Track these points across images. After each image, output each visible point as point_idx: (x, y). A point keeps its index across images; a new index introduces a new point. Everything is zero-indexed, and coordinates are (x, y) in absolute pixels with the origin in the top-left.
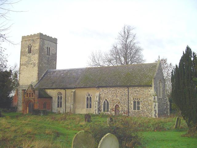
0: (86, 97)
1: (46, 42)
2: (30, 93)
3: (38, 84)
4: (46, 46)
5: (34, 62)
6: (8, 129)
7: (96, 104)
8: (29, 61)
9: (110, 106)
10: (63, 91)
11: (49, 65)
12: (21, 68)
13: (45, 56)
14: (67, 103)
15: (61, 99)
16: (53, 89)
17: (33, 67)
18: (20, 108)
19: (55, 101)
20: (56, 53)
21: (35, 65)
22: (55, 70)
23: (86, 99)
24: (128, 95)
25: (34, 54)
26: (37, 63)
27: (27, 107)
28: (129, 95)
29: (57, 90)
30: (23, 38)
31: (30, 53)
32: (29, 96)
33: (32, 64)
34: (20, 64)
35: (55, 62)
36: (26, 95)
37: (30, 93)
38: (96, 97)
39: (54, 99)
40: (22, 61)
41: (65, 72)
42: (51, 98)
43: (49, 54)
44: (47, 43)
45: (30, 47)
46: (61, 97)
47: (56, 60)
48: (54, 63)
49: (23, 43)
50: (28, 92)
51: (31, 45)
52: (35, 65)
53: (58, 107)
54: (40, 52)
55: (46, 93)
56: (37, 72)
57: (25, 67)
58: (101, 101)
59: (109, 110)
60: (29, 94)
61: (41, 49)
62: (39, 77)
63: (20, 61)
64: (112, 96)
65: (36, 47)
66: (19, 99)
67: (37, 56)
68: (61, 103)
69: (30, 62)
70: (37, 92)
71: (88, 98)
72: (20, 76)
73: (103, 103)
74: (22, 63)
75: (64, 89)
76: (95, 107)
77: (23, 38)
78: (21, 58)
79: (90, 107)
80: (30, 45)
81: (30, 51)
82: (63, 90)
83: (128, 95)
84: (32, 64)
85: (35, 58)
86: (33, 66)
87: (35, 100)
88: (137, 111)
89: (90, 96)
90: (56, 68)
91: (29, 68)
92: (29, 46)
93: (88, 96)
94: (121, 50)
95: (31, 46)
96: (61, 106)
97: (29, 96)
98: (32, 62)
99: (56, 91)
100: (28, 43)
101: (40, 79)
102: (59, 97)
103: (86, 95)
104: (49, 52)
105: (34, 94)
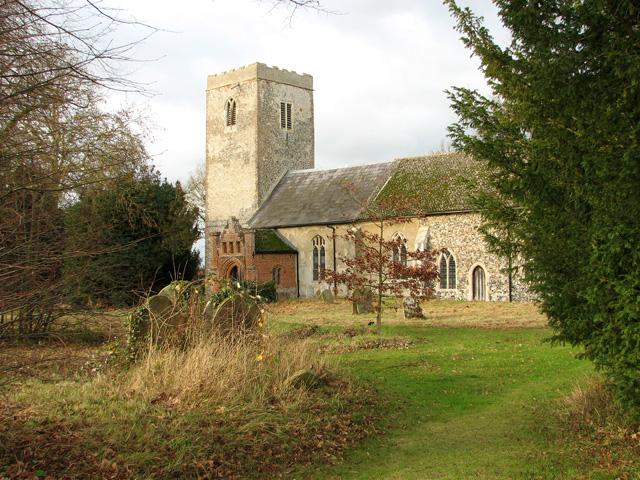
2: (231, 243)
4: (278, 100)
10: (325, 232)
15: (323, 254)
16: (299, 226)
20: (312, 120)
21: (247, 161)
29: (310, 229)
31: (233, 123)
32: (235, 249)
36: (221, 250)
37: (231, 243)
39: (302, 255)
40: (210, 149)
41: (335, 175)
43: (289, 124)
44: (282, 94)
45: (231, 107)
46: (323, 248)
47: (311, 141)
50: (225, 240)
54: (259, 119)
55: (280, 241)
56: (255, 179)
57: (220, 165)
59: (457, 282)
61: (263, 112)
62: (260, 196)
63: (207, 151)
65: (248, 103)
70: (250, 239)
74: (211, 155)
75: (329, 225)
81: (232, 121)
84: (239, 156)
87: (244, 262)
90: (312, 165)
98: (239, 150)
99: (306, 232)
101: (265, 198)
104: (289, 119)
105: (241, 244)
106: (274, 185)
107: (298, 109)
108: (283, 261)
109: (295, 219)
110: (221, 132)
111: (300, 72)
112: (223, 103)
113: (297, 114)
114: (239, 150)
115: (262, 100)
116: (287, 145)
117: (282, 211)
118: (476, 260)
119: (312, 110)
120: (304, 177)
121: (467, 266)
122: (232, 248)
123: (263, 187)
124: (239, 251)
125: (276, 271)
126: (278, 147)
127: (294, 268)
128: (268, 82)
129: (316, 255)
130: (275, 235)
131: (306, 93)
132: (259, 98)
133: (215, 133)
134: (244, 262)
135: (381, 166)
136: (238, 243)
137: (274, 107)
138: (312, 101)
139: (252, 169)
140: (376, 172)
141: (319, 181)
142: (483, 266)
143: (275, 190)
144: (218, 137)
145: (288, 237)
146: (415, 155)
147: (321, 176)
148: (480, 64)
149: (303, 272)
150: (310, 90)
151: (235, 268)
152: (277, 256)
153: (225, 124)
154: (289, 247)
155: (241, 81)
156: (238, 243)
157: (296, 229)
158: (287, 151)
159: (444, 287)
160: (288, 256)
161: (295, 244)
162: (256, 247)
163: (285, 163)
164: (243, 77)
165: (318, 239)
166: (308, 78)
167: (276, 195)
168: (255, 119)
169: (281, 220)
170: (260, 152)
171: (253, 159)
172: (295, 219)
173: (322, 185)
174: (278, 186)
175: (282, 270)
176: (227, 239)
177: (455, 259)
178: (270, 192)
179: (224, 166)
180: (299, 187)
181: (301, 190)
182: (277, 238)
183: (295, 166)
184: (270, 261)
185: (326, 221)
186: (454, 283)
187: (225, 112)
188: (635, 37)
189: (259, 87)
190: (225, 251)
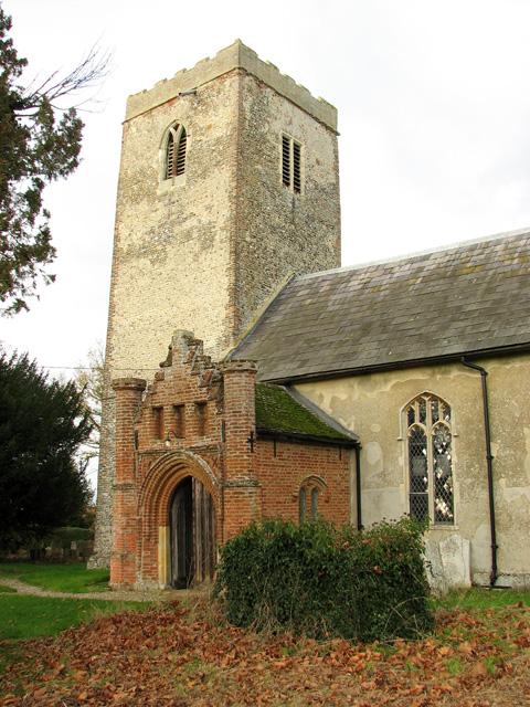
1: (275, 104)
2: (178, 408)
3: (174, 506)
5: (205, 220)
6: (494, 461)
8: (173, 224)
10: (456, 386)
14: (501, 483)
16: (365, 372)
19: (383, 475)
20: (336, 186)
25: (204, 175)
26: (221, 223)
27: (153, 524)
29: (396, 379)
31: (179, 172)
32: (168, 425)
33: (188, 235)
34: (116, 251)
36: (145, 428)
37: (178, 408)
39: (372, 453)
40: (124, 233)
41: (430, 265)
42: (349, 446)
43: (297, 182)
44: (283, 121)
45: (176, 140)
47: (335, 226)
48: (330, 244)
50: (159, 400)
51: (184, 123)
52: (207, 243)
54: (241, 152)
55: (309, 416)
56: (226, 281)
57: (144, 262)
60: (168, 410)
61: (248, 140)
62: (238, 317)
63: (117, 238)
65: (218, 122)
69: (177, 229)
70: (240, 392)
72: (117, 328)
74: (124, 245)
75: (470, 360)
80: (176, 128)
81: (176, 165)
82: (455, 372)
84: (188, 235)
87: (220, 464)
91: (170, 265)
97: (168, 425)
98: (188, 225)
99: (387, 388)
100: (163, 121)
101: (249, 326)
105: (212, 408)
106: (268, 300)
107: (313, 161)
108: (323, 464)
111: (316, 94)
114: (188, 225)
115: (248, 115)
116: (292, 222)
119: (336, 169)
122: (180, 423)
123: (244, 300)
124: (202, 433)
125: (309, 491)
126: (277, 220)
127: (346, 491)
128: (260, 83)
129: (416, 447)
130: (291, 402)
131: (326, 135)
132: (241, 109)
133: (136, 200)
134: (220, 464)
136: (201, 405)
143: (271, 309)
144: (144, 206)
145: (325, 406)
148: (87, 471)
151: (186, 485)
152: (309, 451)
153: (161, 175)
154: (332, 430)
155: (198, 83)
156: (201, 405)
157: (354, 382)
158: (293, 234)
160: (334, 454)
161: (349, 425)
162: (258, 416)
165: (424, 407)
167: (276, 319)
168: (233, 150)
169: (303, 363)
170: (240, 221)
171: (221, 236)
172: (347, 356)
174: (277, 302)
176: (165, 398)
182: (298, 406)
183: (307, 269)
184: (294, 466)
185: (457, 348)
187: (161, 154)
189: (242, 87)
190: (159, 435)
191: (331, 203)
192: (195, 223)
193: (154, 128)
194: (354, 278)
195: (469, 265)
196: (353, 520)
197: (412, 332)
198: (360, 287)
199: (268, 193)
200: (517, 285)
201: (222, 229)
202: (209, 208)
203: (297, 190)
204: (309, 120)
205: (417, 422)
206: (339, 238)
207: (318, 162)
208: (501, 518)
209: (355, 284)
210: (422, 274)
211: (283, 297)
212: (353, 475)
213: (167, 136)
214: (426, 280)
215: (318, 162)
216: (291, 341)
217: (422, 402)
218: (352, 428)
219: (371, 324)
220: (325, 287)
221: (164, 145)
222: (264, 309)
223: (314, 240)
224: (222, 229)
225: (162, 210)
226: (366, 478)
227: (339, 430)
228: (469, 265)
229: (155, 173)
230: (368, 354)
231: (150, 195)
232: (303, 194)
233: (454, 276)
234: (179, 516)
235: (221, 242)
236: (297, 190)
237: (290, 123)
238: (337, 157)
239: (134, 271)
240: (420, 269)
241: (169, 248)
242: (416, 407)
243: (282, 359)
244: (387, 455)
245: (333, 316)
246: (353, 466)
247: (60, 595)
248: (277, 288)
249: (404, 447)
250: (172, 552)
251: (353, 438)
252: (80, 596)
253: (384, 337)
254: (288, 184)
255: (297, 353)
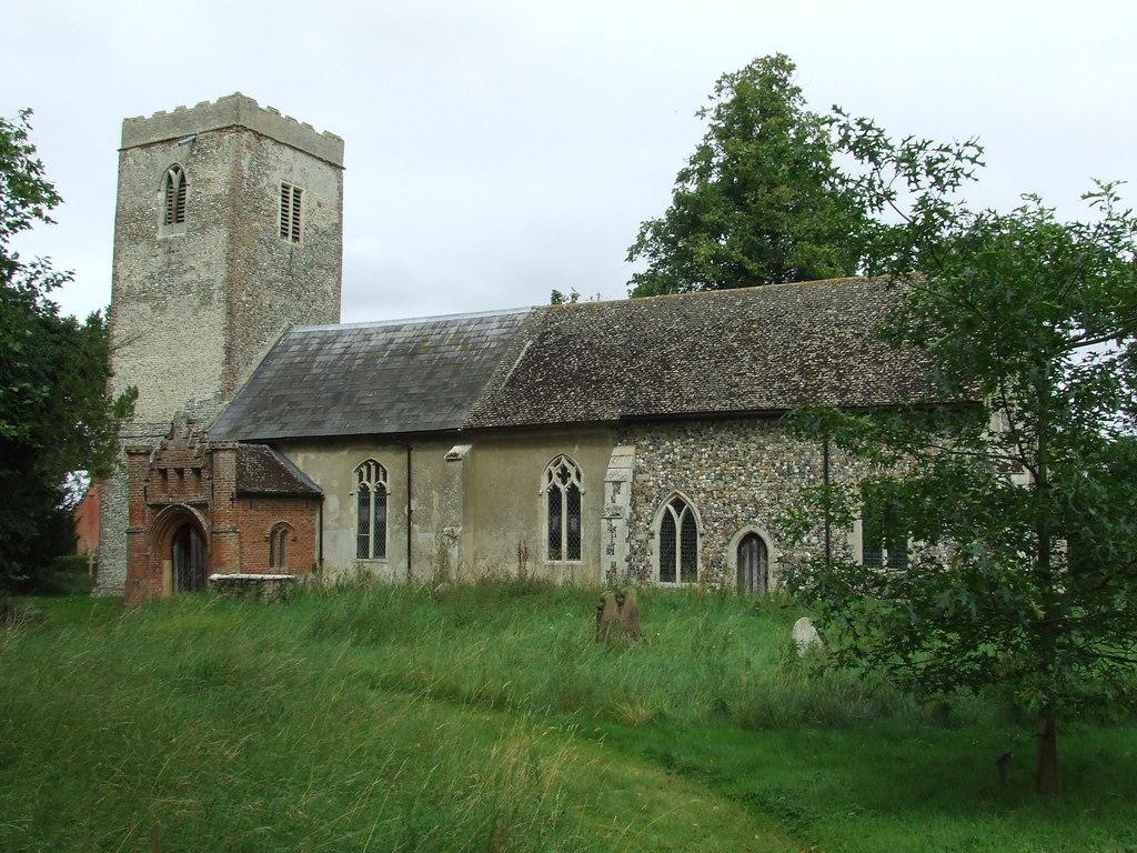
0: (545, 486)
2: (180, 472)
4: (277, 178)
7: (612, 530)
8: (173, 273)
9: (706, 544)
10: (391, 461)
11: (299, 297)
12: (276, 148)
13: (272, 242)
14: (416, 527)
15: (381, 502)
17: (196, 311)
18: (115, 573)
20: (338, 227)
21: (206, 300)
22: (331, 328)
23: (544, 503)
24: (826, 470)
26: (219, 283)
28: (833, 469)
30: (132, 128)
31: (180, 220)
35: (332, 280)
38: (609, 488)
39: (331, 503)
40: (124, 273)
41: (399, 337)
42: (315, 499)
43: (296, 231)
44: (286, 168)
45: (176, 185)
46: (381, 489)
47: (336, 269)
49: (131, 160)
52: (206, 300)
53: (363, 551)
57: (144, 307)
58: (646, 510)
59: (700, 566)
60: (171, 472)
64: (719, 477)
66: (109, 515)
67: (219, 237)
68: (381, 526)
69: (177, 280)
71: (555, 493)
73: (656, 527)
74: (124, 286)
76: (611, 551)
77: (132, 128)
78: (116, 258)
79: (574, 553)
80: (176, 170)
81: (176, 213)
83: (826, 470)
84: (187, 288)
85: (207, 254)
86: (196, 303)
88: (678, 584)
89: (573, 479)
90: (335, 318)
92: (170, 179)
93: (557, 481)
94: (654, 255)
95: (183, 179)
96: (380, 551)
98: (188, 277)
100: (163, 159)
102: (364, 491)
103: (547, 478)
104: (296, 220)
105: (205, 474)
106: (262, 354)
107: (314, 204)
108: (292, 517)
109: (318, 424)
110: (149, 237)
112: (156, 177)
113: (312, 212)
114: (188, 277)
115: (246, 173)
117: (285, 406)
118: (747, 521)
119: (340, 208)
120: (328, 340)
121: (726, 533)
124: (199, 488)
127: (312, 532)
128: (259, 136)
129: (364, 503)
131: (330, 172)
135: (502, 320)
137: (268, 191)
138: (340, 189)
139: (216, 316)
140: (493, 331)
141: (365, 346)
142: (764, 534)
144: (142, 248)
146: (441, 326)
147: (368, 338)
149: (334, 540)
150: (338, 167)
153: (161, 219)
159: (559, 558)
163: (285, 310)
164: (205, 123)
166: (335, 142)
173: (371, 356)
174: (270, 356)
175: (290, 535)
177: (698, 516)
178: (253, 367)
179: (154, 309)
180: (319, 359)
181: (325, 365)
183: (299, 322)
186: (693, 569)
187: (161, 196)
188: (6, 383)
191: (332, 244)
192: (194, 277)
193: (152, 165)
194: (340, 338)
195: (427, 344)
196: (317, 557)
197: (368, 408)
198: (342, 350)
199: (265, 249)
200: (449, 373)
201: (221, 289)
202: (208, 264)
203: (296, 239)
204: (309, 162)
205: (365, 481)
206: (340, 279)
207: (319, 205)
208: (415, 555)
209: (338, 347)
210: (392, 347)
211: (277, 350)
212: (318, 519)
213: (166, 177)
214: (394, 354)
215: (319, 205)
216: (279, 400)
217: (369, 466)
218: (318, 483)
219: (341, 393)
220: (314, 346)
221: (163, 188)
222: (258, 363)
223: (311, 287)
224: (221, 289)
225: (157, 262)
226: (328, 522)
227: (309, 484)
228: (427, 344)
229: (153, 217)
230: (334, 425)
231: (149, 237)
232: (302, 241)
233: (414, 354)
234: (180, 552)
235: (219, 301)
236: (296, 239)
237: (291, 170)
238: (341, 194)
239: (133, 314)
240: (391, 341)
241: (169, 297)
242: (364, 469)
243: (269, 419)
244: (343, 506)
245: (315, 380)
246: (318, 515)
247: (240, 576)
248: (271, 341)
249: (355, 501)
250: (173, 579)
251: (318, 490)
252: (253, 576)
253: (347, 409)
254: (286, 235)
255: (280, 415)
